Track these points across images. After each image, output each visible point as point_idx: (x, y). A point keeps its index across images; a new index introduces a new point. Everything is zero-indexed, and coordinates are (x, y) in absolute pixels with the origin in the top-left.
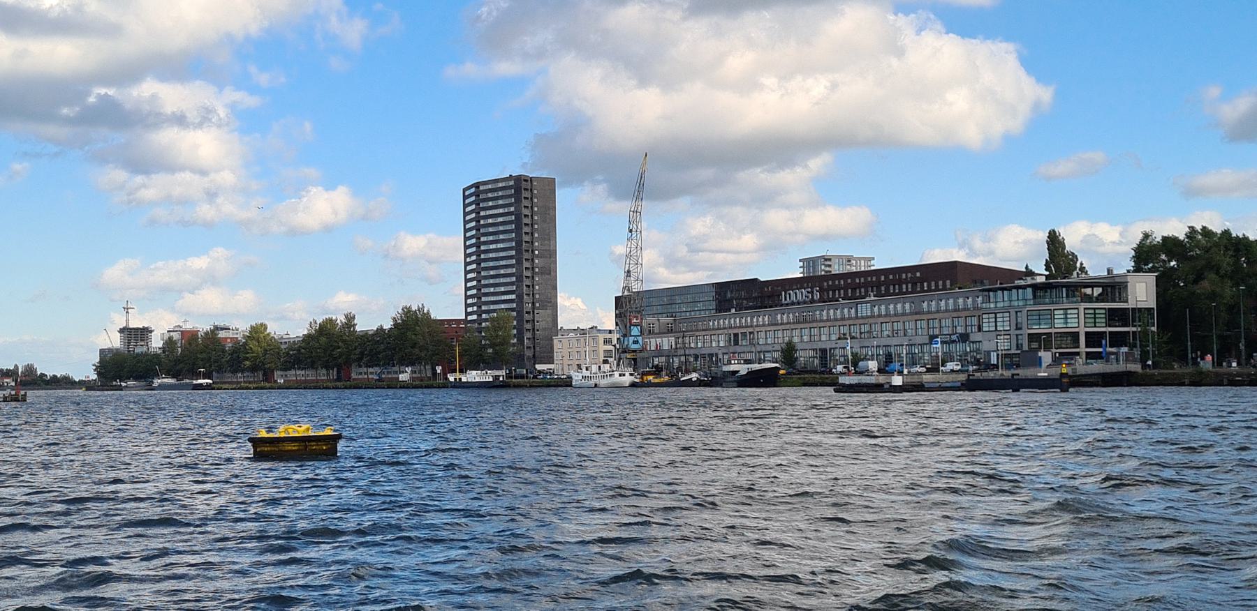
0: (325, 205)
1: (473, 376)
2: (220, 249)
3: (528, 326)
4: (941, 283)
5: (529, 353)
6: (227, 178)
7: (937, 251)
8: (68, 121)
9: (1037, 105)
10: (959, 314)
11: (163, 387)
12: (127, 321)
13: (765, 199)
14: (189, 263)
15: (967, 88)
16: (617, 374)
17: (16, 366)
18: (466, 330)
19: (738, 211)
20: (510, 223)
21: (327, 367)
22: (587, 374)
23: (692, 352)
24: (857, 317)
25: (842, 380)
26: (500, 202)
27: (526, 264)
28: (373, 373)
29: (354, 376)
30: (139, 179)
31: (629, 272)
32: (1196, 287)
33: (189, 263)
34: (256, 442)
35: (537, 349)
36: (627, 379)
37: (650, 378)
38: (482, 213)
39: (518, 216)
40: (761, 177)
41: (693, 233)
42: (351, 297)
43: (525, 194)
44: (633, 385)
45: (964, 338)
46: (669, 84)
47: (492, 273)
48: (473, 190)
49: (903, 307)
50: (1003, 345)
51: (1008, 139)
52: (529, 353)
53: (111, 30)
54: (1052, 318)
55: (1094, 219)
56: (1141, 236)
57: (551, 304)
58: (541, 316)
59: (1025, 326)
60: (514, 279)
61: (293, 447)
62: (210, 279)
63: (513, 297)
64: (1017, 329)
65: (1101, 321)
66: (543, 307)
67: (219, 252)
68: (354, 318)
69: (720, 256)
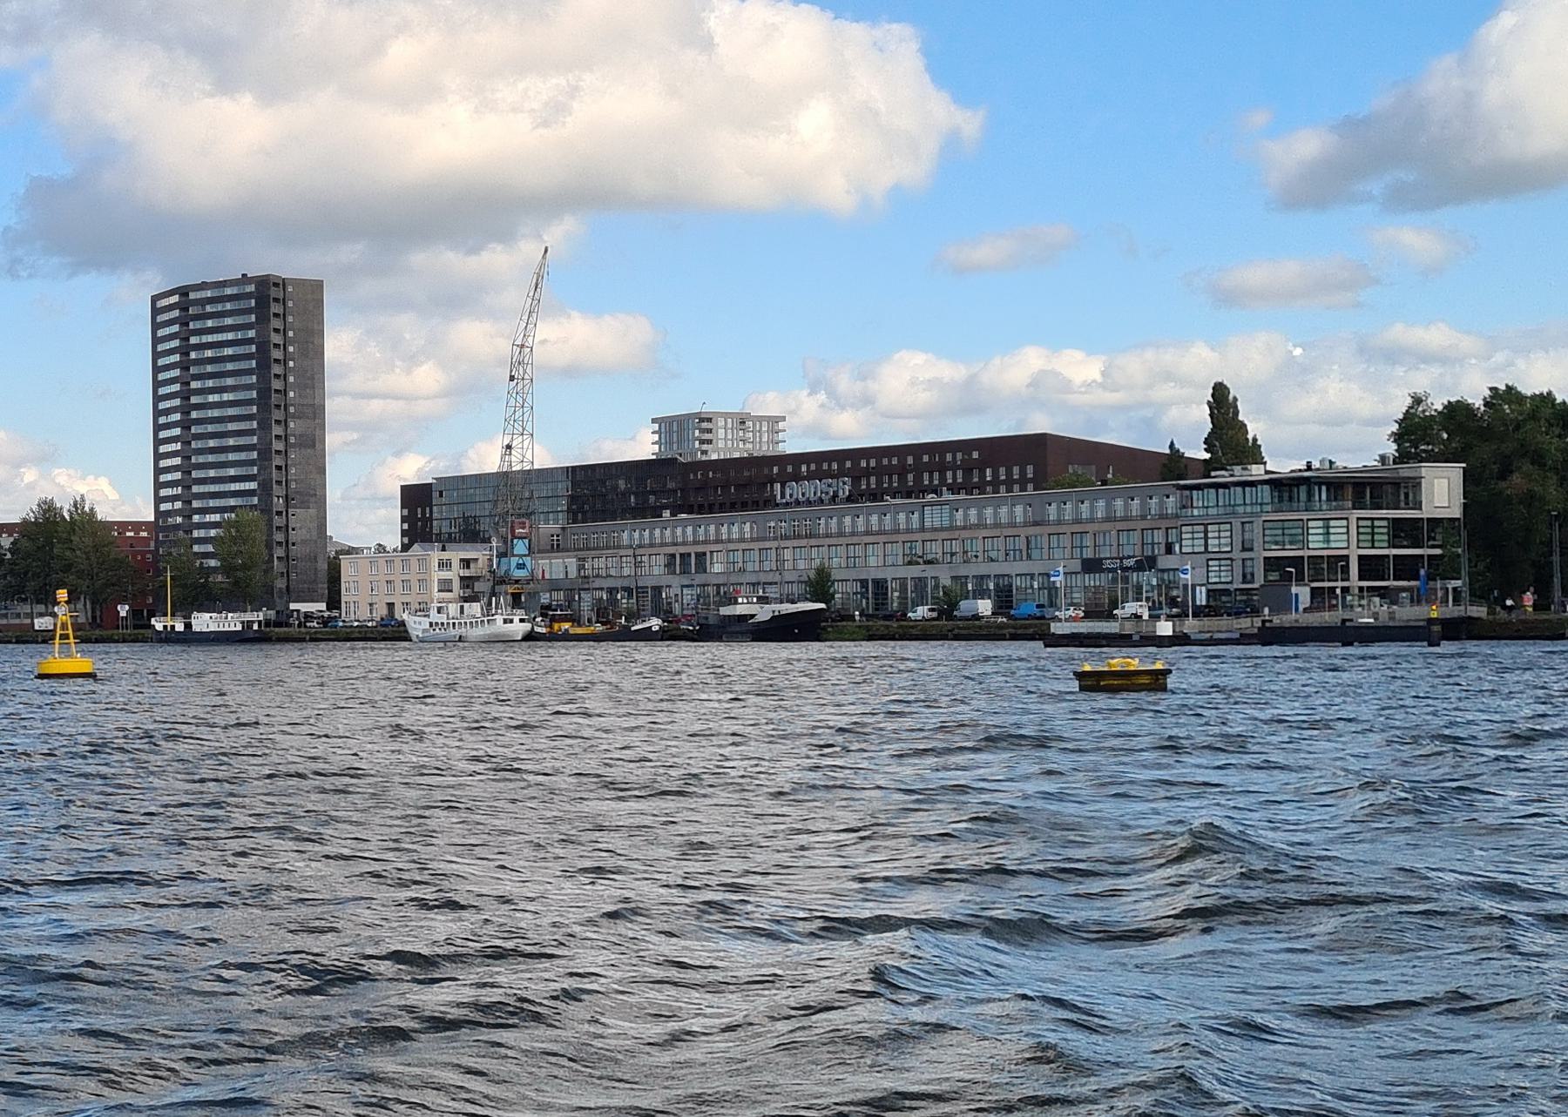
1: (204, 622)
3: (279, 537)
4: (1016, 470)
5: (280, 584)
7: (771, 396)
9: (951, 143)
10: (1131, 525)
13: (457, 300)
16: (499, 619)
19: (407, 325)
20: (241, 352)
22: (442, 618)
23: (619, 584)
24: (923, 529)
26: (229, 321)
27: (277, 430)
31: (509, 447)
32: (1503, 484)
34: (1080, 676)
35: (293, 576)
36: (519, 628)
37: (566, 626)
38: (194, 340)
39: (263, 347)
40: (450, 262)
43: (275, 308)
44: (530, 637)
45: (1147, 563)
46: (273, 91)
47: (212, 443)
48: (175, 299)
49: (1011, 513)
50: (1220, 576)
52: (280, 584)
54: (1305, 531)
56: (1409, 401)
57: (314, 497)
58: (300, 519)
60: (255, 455)
61: (1145, 680)
63: (253, 485)
64: (1244, 549)
65: (1382, 537)
66: (305, 505)
69: (376, 405)
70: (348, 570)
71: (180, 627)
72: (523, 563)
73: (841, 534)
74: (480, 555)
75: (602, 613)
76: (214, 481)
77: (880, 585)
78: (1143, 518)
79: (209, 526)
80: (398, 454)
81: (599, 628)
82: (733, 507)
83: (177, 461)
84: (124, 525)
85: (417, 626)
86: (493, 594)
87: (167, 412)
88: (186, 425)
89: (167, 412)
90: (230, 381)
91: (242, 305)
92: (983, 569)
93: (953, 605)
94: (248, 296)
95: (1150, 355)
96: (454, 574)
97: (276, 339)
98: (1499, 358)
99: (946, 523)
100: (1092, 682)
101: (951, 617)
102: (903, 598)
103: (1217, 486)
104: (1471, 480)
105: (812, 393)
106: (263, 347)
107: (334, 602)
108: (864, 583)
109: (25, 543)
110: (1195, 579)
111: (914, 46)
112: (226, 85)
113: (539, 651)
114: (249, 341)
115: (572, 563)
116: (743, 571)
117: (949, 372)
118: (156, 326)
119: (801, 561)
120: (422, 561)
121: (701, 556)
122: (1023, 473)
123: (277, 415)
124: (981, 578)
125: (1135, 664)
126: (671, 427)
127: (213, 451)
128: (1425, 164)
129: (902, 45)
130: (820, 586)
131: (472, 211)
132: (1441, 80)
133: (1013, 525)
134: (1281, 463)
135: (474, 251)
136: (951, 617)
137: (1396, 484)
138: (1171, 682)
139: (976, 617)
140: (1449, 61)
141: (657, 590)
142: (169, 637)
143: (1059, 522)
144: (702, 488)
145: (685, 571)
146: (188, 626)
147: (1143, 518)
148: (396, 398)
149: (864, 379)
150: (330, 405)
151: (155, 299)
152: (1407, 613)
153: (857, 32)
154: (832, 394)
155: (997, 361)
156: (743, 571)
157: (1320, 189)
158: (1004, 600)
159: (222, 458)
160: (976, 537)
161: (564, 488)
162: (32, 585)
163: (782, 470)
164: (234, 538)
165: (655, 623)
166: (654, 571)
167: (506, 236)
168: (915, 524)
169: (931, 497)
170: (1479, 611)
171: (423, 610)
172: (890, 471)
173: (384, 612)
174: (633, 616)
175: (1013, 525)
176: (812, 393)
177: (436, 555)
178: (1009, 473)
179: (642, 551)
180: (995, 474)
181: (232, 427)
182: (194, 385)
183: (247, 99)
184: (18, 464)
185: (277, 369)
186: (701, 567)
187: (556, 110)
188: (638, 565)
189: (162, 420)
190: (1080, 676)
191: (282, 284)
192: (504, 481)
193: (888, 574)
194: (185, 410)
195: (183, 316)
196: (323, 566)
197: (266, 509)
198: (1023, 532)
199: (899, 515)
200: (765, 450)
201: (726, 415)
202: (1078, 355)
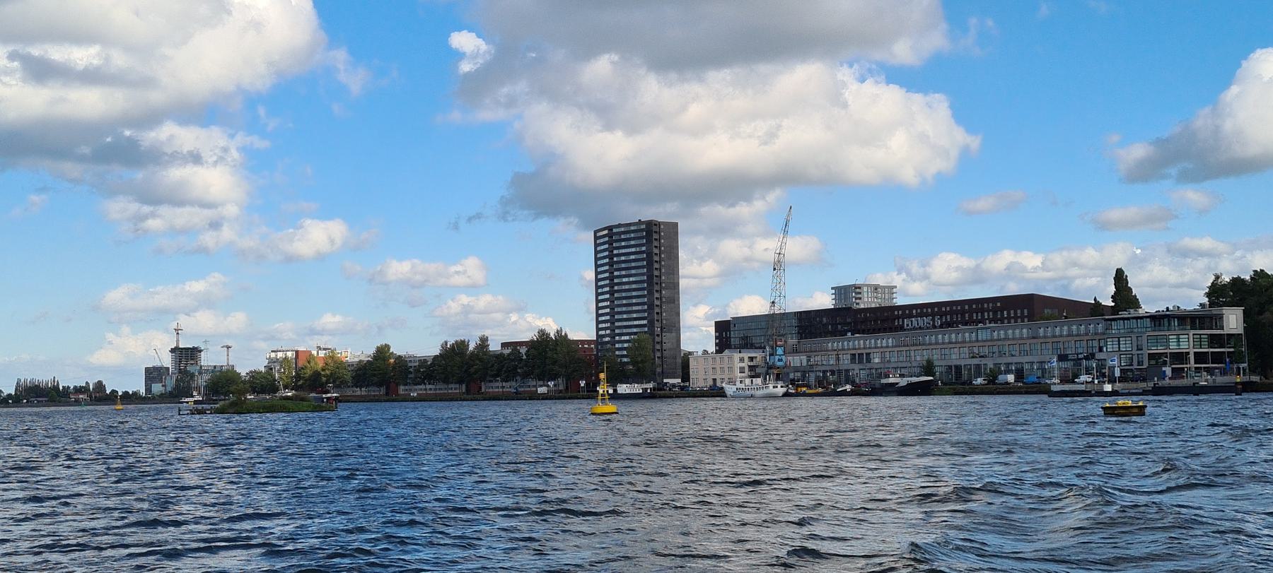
0: (319, 235)
1: (623, 389)
2: (216, 275)
3: (658, 347)
5: (659, 370)
6: (232, 210)
7: (879, 275)
8: (82, 159)
9: (965, 152)
12: (178, 341)
13: (724, 230)
14: (187, 288)
15: (894, 131)
18: (585, 350)
21: (460, 382)
22: (742, 386)
25: (1054, 388)
27: (657, 295)
28: (510, 387)
30: (146, 209)
33: (187, 288)
34: (1104, 409)
36: (780, 390)
39: (650, 255)
42: (338, 318)
43: (656, 236)
44: (786, 395)
45: (1091, 356)
46: (632, 129)
48: (606, 232)
51: (939, 177)
52: (659, 370)
53: (146, 82)
54: (1168, 341)
55: (1018, 249)
57: (674, 327)
58: (668, 338)
59: (1145, 347)
62: (205, 302)
63: (645, 322)
67: (217, 277)
68: (487, 339)
70: (692, 363)
72: (782, 358)
73: (937, 343)
74: (758, 355)
75: (820, 383)
77: (958, 368)
78: (1087, 334)
80: (695, 305)
81: (820, 390)
82: (879, 331)
83: (608, 310)
84: (583, 342)
85: (730, 390)
86: (767, 373)
87: (602, 287)
88: (612, 293)
89: (602, 287)
90: (633, 272)
91: (639, 235)
92: (1010, 360)
93: (996, 378)
94: (642, 230)
95: (1065, 253)
96: (745, 364)
97: (656, 251)
98: (1238, 254)
100: (1109, 412)
101: (995, 384)
102: (970, 374)
103: (1124, 319)
104: (1246, 315)
106: (650, 255)
107: (686, 377)
108: (950, 367)
110: (1116, 364)
111: (946, 104)
112: (609, 127)
113: (786, 401)
114: (643, 252)
115: (804, 358)
116: (889, 362)
117: (967, 263)
118: (596, 245)
119: (920, 357)
121: (868, 354)
122: (1022, 313)
124: (1008, 364)
125: (1130, 403)
126: (841, 292)
128: (1199, 160)
129: (942, 103)
130: (928, 368)
131: (731, 187)
132: (1202, 120)
133: (1022, 338)
134: (1147, 308)
135: (733, 205)
136: (995, 384)
137: (1211, 317)
138: (1148, 410)
139: (1007, 383)
140: (1207, 110)
141: (847, 371)
143: (1045, 337)
144: (865, 321)
145: (861, 362)
146: (615, 391)
147: (1087, 334)
148: (695, 278)
149: (924, 266)
150: (683, 283)
151: (595, 232)
152: (1221, 380)
153: (918, 98)
154: (909, 273)
155: (990, 257)
156: (889, 362)
157: (1145, 173)
158: (1020, 375)
160: (1011, 345)
161: (794, 322)
162: (537, 371)
164: (637, 349)
165: (848, 387)
166: (845, 361)
167: (748, 198)
168: (974, 338)
169: (980, 325)
170: (1255, 378)
171: (731, 382)
172: (957, 313)
173: (711, 383)
174: (836, 384)
175: (1022, 338)
177: (737, 356)
179: (837, 352)
180: (1009, 314)
181: (634, 294)
183: (619, 134)
184: (508, 312)
185: (656, 266)
186: (869, 360)
187: (772, 135)
188: (838, 359)
190: (1104, 409)
191: (658, 224)
192: (769, 319)
193: (962, 363)
194: (612, 285)
196: (679, 361)
197: (651, 332)
198: (1028, 342)
199: (966, 334)
200: (887, 304)
201: (868, 286)
202: (1030, 254)
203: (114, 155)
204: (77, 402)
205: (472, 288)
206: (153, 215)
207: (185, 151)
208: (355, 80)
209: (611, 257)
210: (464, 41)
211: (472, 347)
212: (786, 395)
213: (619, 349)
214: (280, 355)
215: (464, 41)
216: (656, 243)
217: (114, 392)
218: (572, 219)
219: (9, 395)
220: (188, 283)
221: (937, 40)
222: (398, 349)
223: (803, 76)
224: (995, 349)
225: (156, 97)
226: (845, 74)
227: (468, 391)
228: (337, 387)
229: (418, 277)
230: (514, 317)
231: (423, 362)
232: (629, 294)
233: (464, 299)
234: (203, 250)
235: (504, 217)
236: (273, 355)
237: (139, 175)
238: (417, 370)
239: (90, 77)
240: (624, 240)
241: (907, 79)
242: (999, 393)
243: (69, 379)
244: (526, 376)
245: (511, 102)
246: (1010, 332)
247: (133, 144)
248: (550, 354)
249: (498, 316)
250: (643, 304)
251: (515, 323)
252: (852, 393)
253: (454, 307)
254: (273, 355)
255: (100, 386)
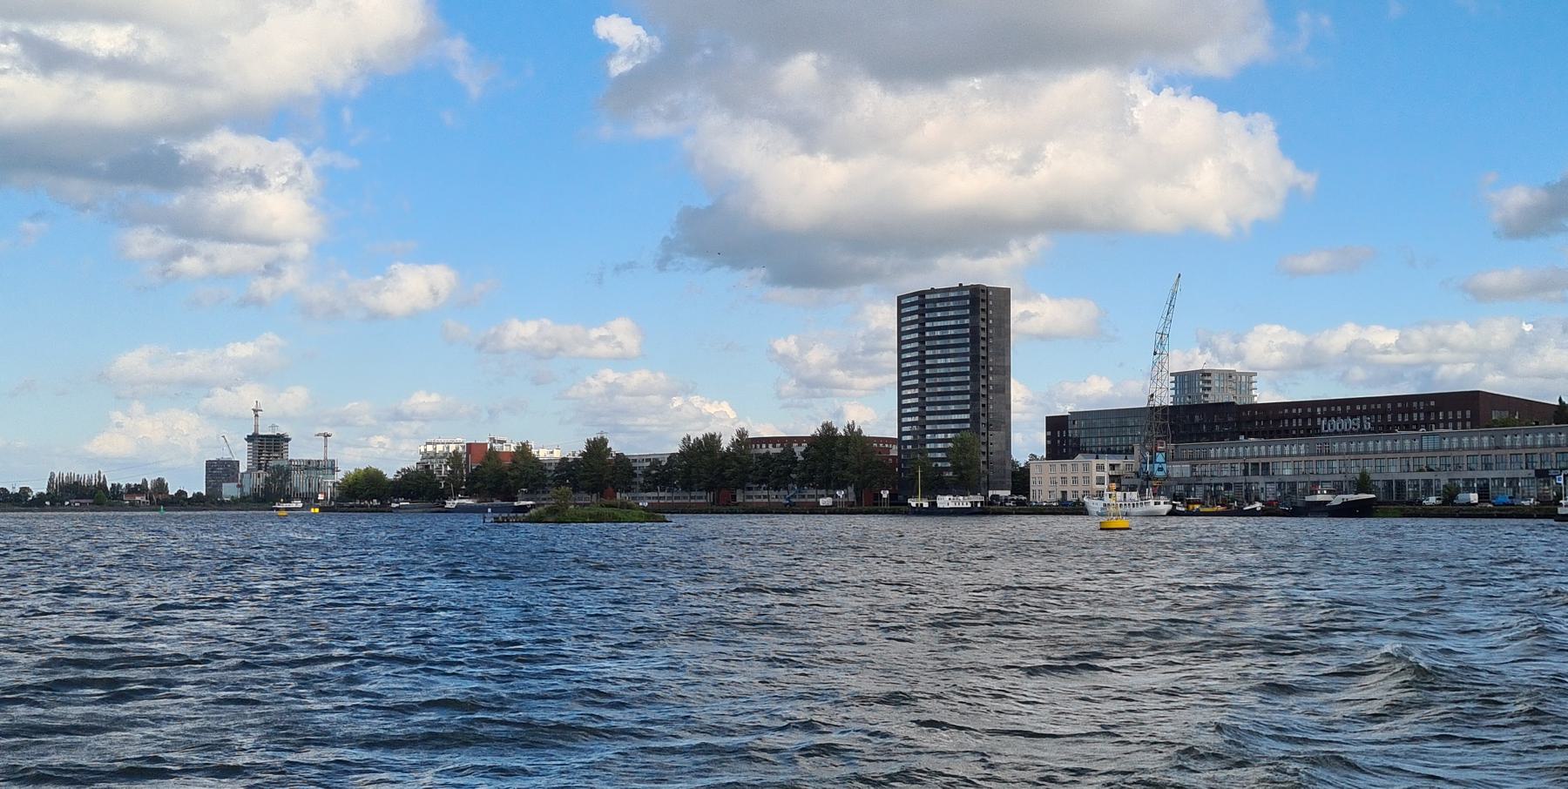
0: (415, 285)
1: (944, 501)
6: (299, 249)
9: (1294, 193)
11: (460, 509)
12: (256, 426)
14: (230, 353)
17: (145, 481)
21: (708, 489)
26: (952, 313)
27: (983, 382)
28: (775, 497)
29: (739, 499)
33: (230, 353)
36: (1164, 507)
38: (928, 325)
39: (975, 331)
41: (874, 325)
42: (434, 398)
43: (982, 305)
44: (1172, 513)
46: (841, 152)
47: (939, 389)
53: (201, 80)
55: (1364, 323)
58: (995, 436)
63: (966, 416)
71: (926, 505)
76: (940, 413)
79: (938, 445)
81: (1220, 508)
84: (879, 440)
88: (922, 378)
90: (952, 351)
91: (961, 303)
92: (1470, 475)
93: (1454, 496)
94: (965, 298)
96: (1105, 474)
97: (983, 325)
99: (1437, 446)
105: (1203, 352)
106: (975, 331)
109: (813, 451)
111: (1271, 127)
112: (810, 148)
114: (965, 326)
117: (1296, 339)
120: (1087, 468)
121: (1265, 465)
122: (1464, 414)
123: (983, 372)
124: (1467, 481)
127: (940, 394)
129: (1265, 125)
130: (1363, 484)
139: (1469, 504)
142: (919, 512)
144: (1252, 420)
151: (900, 299)
153: (1232, 117)
158: (1484, 496)
159: (946, 399)
163: (1304, 411)
165: (1258, 506)
173: (1060, 496)
175: (1534, 447)
176: (1203, 352)
177: (1094, 462)
178: (1455, 414)
180: (1446, 415)
181: (953, 379)
182: (928, 353)
184: (670, 394)
185: (983, 344)
187: (1032, 158)
189: (904, 374)
191: (985, 290)
193: (1407, 477)
195: (919, 310)
199: (1405, 441)
200: (1246, 401)
203: (146, 169)
204: (134, 506)
205: (622, 361)
206: (191, 252)
207: (243, 168)
208: (473, 78)
209: (922, 331)
210: (617, 29)
211: (725, 444)
212: (1172, 513)
213: (931, 450)
214: (440, 448)
215: (617, 29)
216: (983, 315)
217: (181, 493)
218: (755, 271)
219: (40, 495)
220: (231, 345)
221: (1254, 46)
222: (616, 446)
223: (1075, 89)
224: (1449, 460)
225: (212, 99)
226: (1137, 85)
227: (716, 502)
228: (531, 493)
229: (547, 344)
230: (678, 402)
231: (655, 462)
232: (945, 380)
233: (610, 376)
234: (259, 302)
235: (662, 264)
236: (430, 448)
237: (178, 201)
238: (646, 473)
239: (118, 68)
240: (940, 310)
241: (1229, 94)
242: (1511, 517)
243: (117, 478)
244: (802, 483)
245: (674, 114)
246: (1465, 439)
247: (171, 157)
248: (838, 455)
249: (655, 399)
250: (966, 393)
251: (679, 409)
252: (1264, 513)
253: (596, 385)
254: (430, 448)
255: (161, 485)
